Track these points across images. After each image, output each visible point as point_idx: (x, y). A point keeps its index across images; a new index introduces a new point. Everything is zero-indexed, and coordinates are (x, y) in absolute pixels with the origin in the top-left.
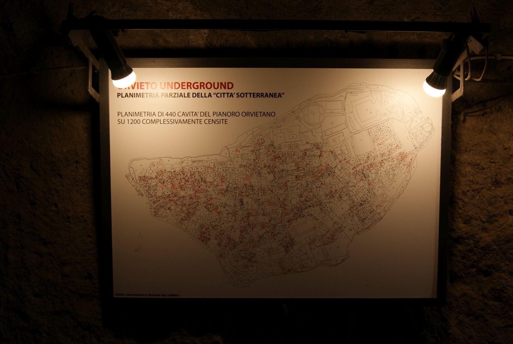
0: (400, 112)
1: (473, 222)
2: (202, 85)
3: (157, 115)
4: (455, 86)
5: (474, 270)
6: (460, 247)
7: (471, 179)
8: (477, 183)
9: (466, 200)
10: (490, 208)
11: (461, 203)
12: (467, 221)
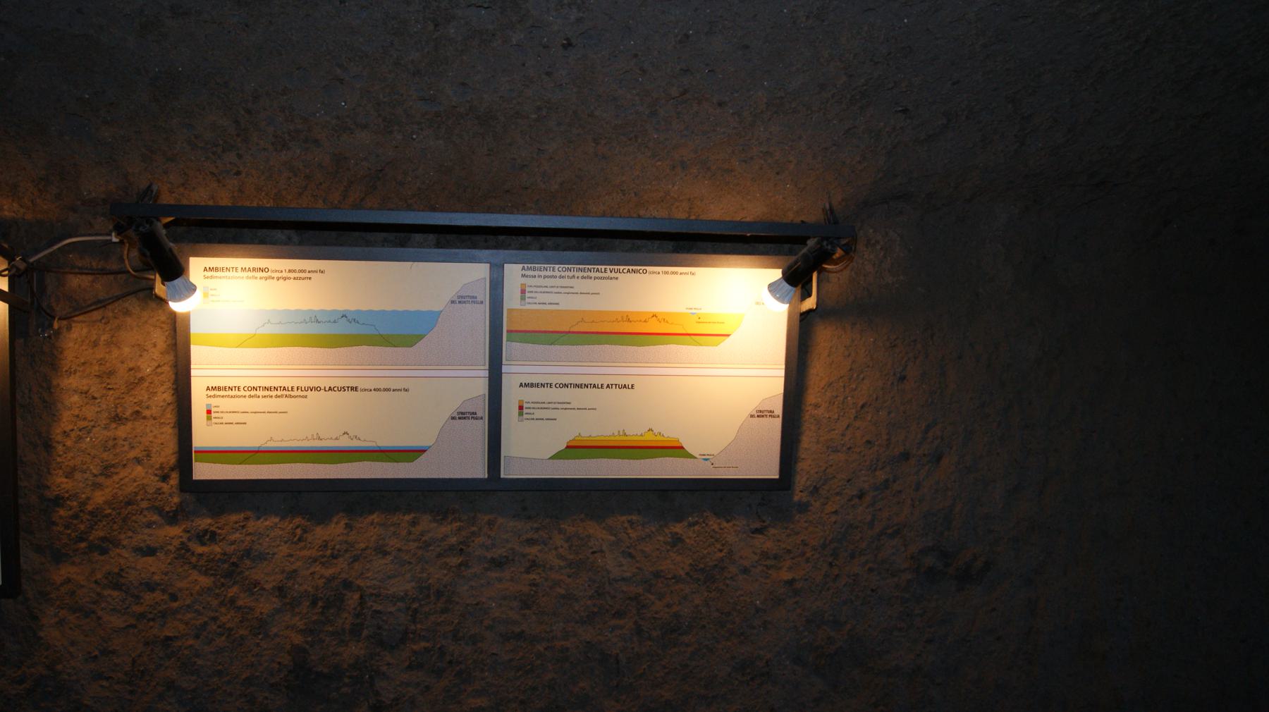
0: (716, 348)
1: (78, 476)
2: (254, 269)
3: (253, 343)
4: (806, 294)
5: (83, 545)
6: (62, 512)
7: (76, 412)
8: (85, 419)
9: (69, 443)
10: (105, 455)
11: (60, 447)
12: (69, 475)
